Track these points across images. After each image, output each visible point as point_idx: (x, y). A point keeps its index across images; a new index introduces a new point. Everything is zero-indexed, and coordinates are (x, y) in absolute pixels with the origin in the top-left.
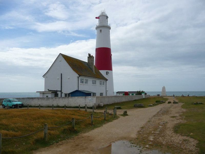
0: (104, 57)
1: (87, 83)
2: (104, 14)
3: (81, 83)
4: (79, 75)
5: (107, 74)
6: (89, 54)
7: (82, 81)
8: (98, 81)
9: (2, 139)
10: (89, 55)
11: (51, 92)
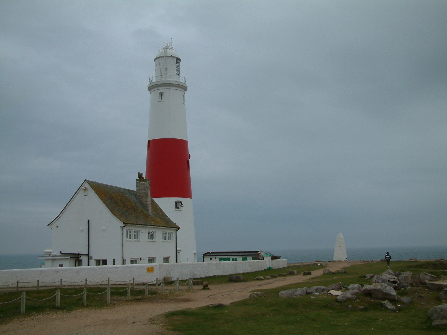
0: (169, 164)
1: (138, 238)
2: (170, 52)
4: (124, 223)
5: (177, 208)
6: (139, 173)
7: (129, 233)
8: (159, 233)
11: (69, 258)
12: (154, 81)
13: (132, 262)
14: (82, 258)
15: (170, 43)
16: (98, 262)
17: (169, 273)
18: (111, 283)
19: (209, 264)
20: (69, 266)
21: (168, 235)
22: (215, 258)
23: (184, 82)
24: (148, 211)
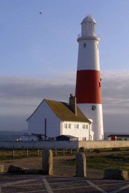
5: (93, 109)
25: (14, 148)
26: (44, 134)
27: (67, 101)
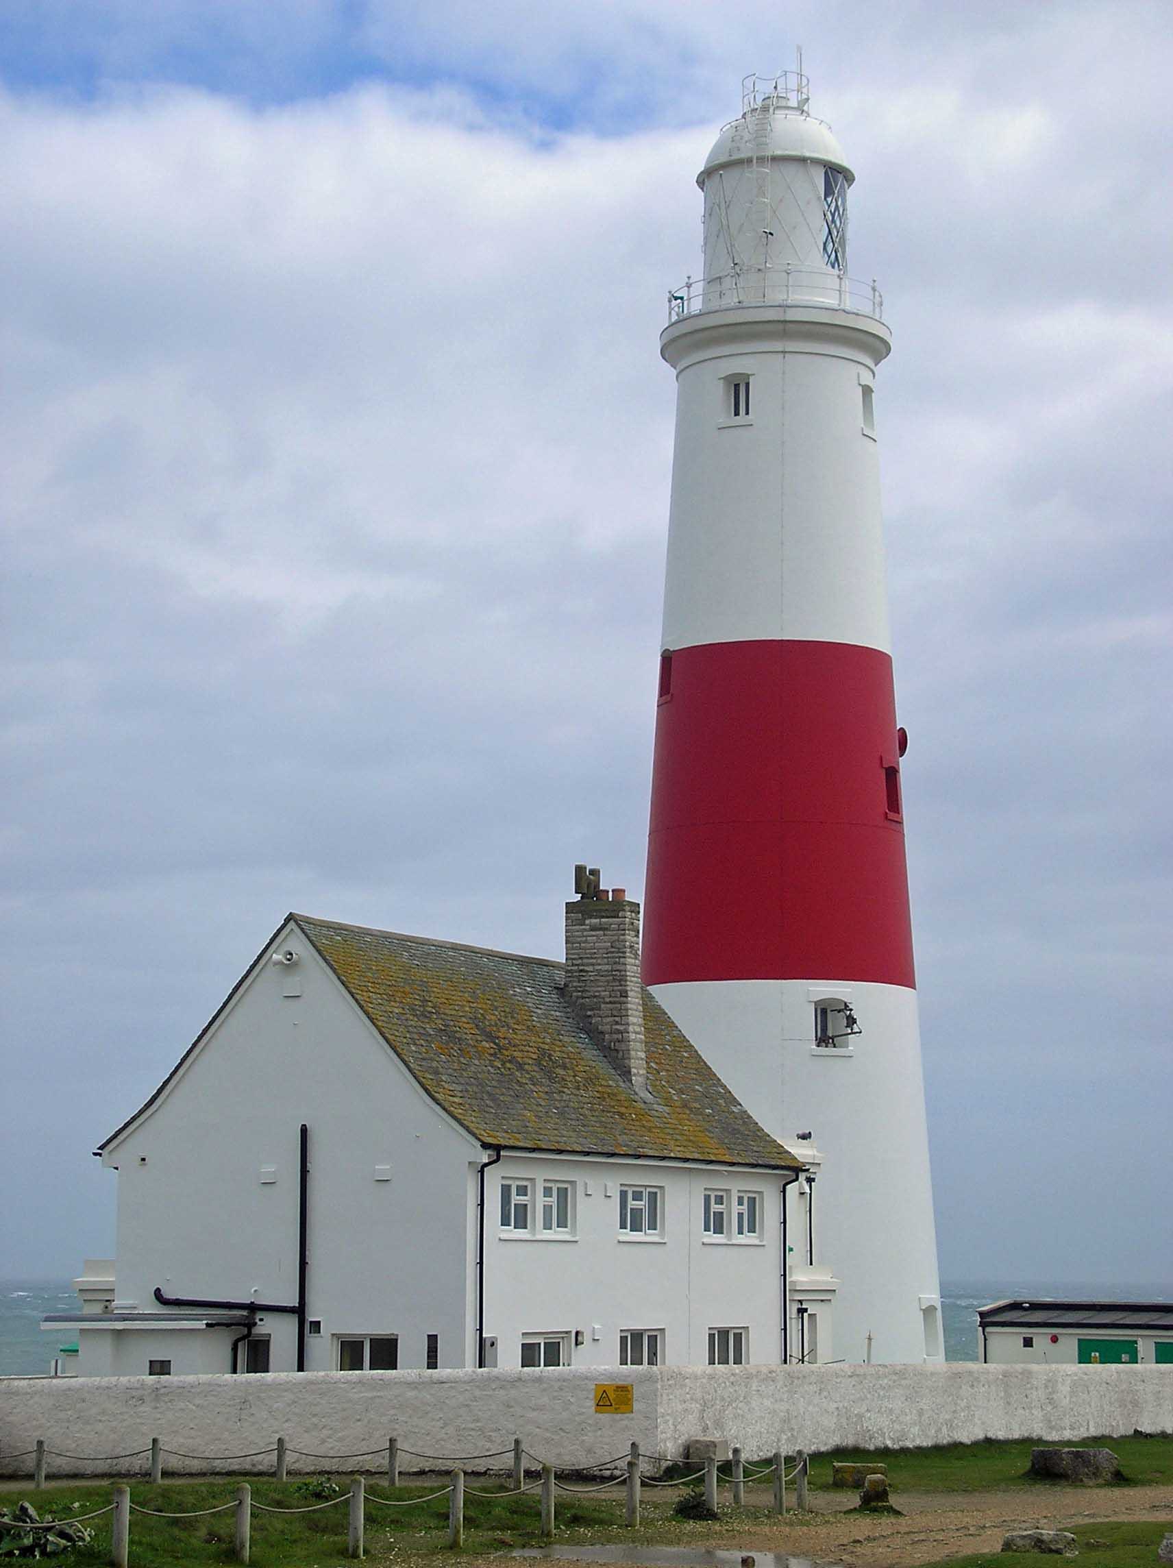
3: (505, 1222)
4: (485, 1146)
5: (824, 1039)
6: (580, 870)
7: (516, 1199)
8: (683, 1200)
9: (347, 1534)
10: (586, 881)
11: (201, 1325)
12: (696, 306)
13: (529, 1355)
14: (267, 1326)
15: (793, 82)
16: (351, 1353)
17: (719, 1424)
18: (404, 1462)
19: (958, 1375)
20: (203, 1367)
21: (736, 1208)
22: (1054, 1339)
23: (866, 309)
24: (626, 1073)
25: (525, 1464)
26: (295, 1302)
27: (548, 941)
